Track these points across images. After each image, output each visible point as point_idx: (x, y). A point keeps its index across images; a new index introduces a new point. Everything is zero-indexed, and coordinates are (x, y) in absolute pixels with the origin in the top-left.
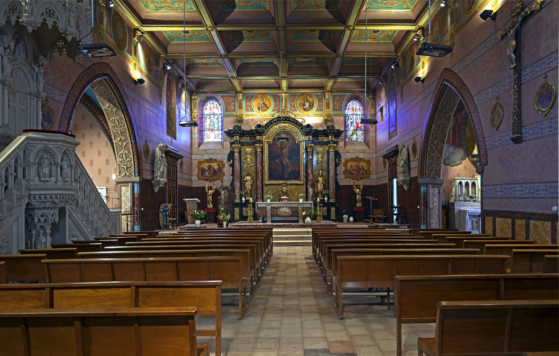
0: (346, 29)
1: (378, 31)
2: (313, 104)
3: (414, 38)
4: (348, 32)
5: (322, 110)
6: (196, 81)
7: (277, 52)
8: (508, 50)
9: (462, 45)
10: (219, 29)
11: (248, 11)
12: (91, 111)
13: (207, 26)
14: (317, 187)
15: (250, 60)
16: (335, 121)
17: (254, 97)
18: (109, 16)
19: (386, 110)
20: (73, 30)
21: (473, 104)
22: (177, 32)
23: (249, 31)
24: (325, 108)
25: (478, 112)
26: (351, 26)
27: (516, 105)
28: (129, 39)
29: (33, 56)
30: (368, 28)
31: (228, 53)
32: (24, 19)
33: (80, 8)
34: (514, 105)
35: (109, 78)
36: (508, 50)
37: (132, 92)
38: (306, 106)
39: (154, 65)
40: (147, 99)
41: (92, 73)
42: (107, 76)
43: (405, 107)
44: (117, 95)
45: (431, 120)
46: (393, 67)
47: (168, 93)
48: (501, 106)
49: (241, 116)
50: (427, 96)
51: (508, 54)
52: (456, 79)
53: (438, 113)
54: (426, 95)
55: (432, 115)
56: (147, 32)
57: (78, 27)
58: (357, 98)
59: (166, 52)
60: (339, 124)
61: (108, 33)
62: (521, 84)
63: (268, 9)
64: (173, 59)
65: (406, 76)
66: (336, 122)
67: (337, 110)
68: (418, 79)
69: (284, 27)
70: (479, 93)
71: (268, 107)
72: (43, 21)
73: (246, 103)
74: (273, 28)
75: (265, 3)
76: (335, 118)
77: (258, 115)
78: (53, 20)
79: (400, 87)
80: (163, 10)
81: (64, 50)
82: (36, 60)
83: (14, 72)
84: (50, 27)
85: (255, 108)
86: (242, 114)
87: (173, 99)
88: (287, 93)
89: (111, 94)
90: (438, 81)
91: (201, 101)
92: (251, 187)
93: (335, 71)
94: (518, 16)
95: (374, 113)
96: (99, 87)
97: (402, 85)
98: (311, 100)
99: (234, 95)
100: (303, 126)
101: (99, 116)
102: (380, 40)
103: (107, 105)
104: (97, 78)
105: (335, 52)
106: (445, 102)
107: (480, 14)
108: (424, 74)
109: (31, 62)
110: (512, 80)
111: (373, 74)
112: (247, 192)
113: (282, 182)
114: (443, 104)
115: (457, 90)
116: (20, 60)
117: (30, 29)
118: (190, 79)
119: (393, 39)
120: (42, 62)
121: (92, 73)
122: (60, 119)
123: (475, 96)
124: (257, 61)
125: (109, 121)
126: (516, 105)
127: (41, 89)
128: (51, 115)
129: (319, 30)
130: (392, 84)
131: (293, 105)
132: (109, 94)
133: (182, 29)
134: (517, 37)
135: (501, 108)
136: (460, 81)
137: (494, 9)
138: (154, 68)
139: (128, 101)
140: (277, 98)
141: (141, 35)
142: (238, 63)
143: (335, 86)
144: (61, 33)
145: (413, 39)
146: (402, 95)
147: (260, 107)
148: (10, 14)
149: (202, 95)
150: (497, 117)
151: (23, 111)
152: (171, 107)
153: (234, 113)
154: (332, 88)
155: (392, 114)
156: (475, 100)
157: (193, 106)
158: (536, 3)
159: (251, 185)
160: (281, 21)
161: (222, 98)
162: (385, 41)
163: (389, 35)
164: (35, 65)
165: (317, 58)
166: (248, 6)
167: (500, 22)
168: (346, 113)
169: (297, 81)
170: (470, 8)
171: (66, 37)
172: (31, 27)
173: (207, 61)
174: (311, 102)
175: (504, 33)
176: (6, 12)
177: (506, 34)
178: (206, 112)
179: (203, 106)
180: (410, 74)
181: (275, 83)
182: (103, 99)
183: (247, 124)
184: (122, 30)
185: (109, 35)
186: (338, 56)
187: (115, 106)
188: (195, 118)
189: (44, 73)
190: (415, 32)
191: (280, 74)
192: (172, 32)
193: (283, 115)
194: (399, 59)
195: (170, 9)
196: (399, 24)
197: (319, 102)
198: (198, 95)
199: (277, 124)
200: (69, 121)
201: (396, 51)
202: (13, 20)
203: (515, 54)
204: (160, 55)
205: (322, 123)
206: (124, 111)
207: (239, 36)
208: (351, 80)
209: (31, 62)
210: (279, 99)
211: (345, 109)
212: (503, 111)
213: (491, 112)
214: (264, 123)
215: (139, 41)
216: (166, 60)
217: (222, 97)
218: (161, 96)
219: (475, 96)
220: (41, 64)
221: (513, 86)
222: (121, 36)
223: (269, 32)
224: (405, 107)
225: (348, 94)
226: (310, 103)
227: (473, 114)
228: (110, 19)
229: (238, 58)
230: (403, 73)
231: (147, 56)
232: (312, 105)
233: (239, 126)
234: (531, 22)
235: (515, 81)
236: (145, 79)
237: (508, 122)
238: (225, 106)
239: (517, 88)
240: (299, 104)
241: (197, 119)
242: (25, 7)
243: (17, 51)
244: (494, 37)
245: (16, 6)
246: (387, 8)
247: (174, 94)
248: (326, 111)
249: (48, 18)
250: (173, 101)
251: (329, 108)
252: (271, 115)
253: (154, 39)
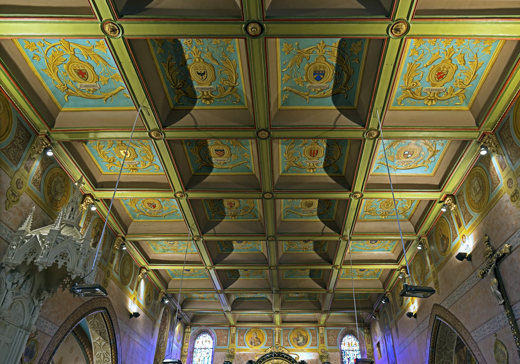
0: (333, 268)
1: (364, 270)
2: (307, 339)
3: (399, 275)
4: (336, 271)
5: (316, 345)
6: (191, 315)
7: (270, 289)
8: (491, 286)
9: (446, 282)
10: (217, 268)
11: (244, 253)
12: (81, 343)
13: (206, 266)
15: (245, 295)
16: (331, 357)
17: (247, 331)
18: (120, 257)
19: (383, 345)
20: (79, 270)
21: (472, 341)
22: (179, 270)
23: (244, 270)
24: (320, 343)
25: (479, 350)
26: (338, 266)
27: (518, 342)
28: (134, 276)
29: (38, 290)
30: (353, 267)
31: (224, 289)
32: (38, 260)
33: (92, 251)
34: (516, 343)
35: (106, 311)
36: (491, 286)
37: (125, 326)
38: (300, 341)
39: (153, 299)
40: (139, 332)
41: (90, 306)
42: (103, 310)
43: (402, 343)
44: (109, 328)
45: (432, 358)
46: (383, 302)
47: (162, 326)
48: (502, 343)
49: (233, 351)
50: (423, 332)
51: (493, 291)
52: (448, 315)
53: (438, 350)
54: (421, 330)
55: (432, 352)
56: (152, 270)
57: (85, 267)
58: (352, 333)
59: (167, 287)
60: (335, 360)
61: (115, 271)
62: (516, 320)
63: (262, 251)
64: (172, 294)
65: (398, 311)
66: (332, 359)
67: (332, 346)
68: (410, 315)
69: (276, 266)
70: (475, 329)
71: (261, 341)
72: (55, 262)
73: (239, 337)
74: (266, 268)
75: (259, 247)
76: (331, 354)
77: (250, 350)
78: (64, 261)
79: (393, 321)
80: (169, 252)
81: (68, 285)
82: (39, 294)
83: (14, 304)
84: (59, 267)
85: (248, 343)
86: (234, 349)
87: (166, 333)
88: (281, 327)
89: (104, 327)
90: (431, 317)
91: (193, 334)
93: (327, 304)
94: (492, 257)
95: (371, 348)
96: (94, 320)
97: (395, 320)
98: (305, 335)
99: (227, 328)
100: (297, 362)
101: (87, 350)
102: (367, 278)
103: (97, 338)
104: (94, 311)
105: (326, 288)
106: (442, 338)
107: (456, 256)
108: (415, 310)
109: (33, 296)
110: (505, 315)
111: (363, 309)
114: (440, 340)
115: (452, 326)
116: (23, 294)
117: (41, 268)
118: (186, 312)
119: (379, 276)
120: (44, 296)
121: (90, 306)
122: (42, 354)
123: (472, 332)
124: (251, 296)
125: (95, 355)
126: (518, 342)
127: (33, 322)
128: (35, 349)
129: (309, 269)
130: (385, 319)
131: (286, 339)
132: (102, 327)
133: (182, 268)
134: (497, 274)
135: (503, 346)
136: (453, 317)
137: (468, 252)
138: (153, 302)
139: (118, 335)
140: (270, 333)
141: (146, 272)
142: (233, 298)
143: (329, 320)
144: (68, 272)
145: (398, 277)
146: (397, 330)
147: (253, 341)
148: (28, 256)
149: (196, 328)
150: (501, 356)
151: (8, 344)
152: (162, 340)
153: (226, 347)
154: (325, 323)
155: (390, 350)
156: (473, 337)
157: (185, 339)
158: (505, 248)
160: (273, 261)
161: (215, 331)
162: (372, 278)
163: (375, 273)
164: (36, 298)
165: (309, 294)
166: (244, 249)
167: (477, 262)
168: (342, 349)
169: (290, 316)
170: (445, 251)
171: (71, 276)
172: (42, 267)
173: (204, 296)
174: (305, 337)
175: (483, 271)
176: (26, 255)
177: (485, 273)
178: (197, 346)
179: (196, 339)
180: (402, 309)
181: (268, 317)
182: (94, 332)
183: (238, 360)
184: (129, 268)
185: (116, 272)
186: (328, 292)
187: (105, 339)
188: (185, 352)
189: (43, 306)
190: (398, 270)
191: (273, 309)
192: (175, 270)
193: (276, 350)
194: (388, 294)
195: (175, 251)
196: (382, 264)
197: (313, 337)
198: (192, 328)
199: (269, 360)
200: (52, 355)
201: (384, 287)
202: (29, 261)
203: (500, 291)
204: (161, 290)
205: (317, 360)
206: (112, 345)
207: (235, 274)
208: (344, 314)
209: (33, 296)
210: (273, 333)
211: (341, 344)
212: (506, 349)
213: (493, 351)
214: (256, 359)
215: (143, 278)
216: (166, 295)
217: (215, 330)
218: (153, 329)
219: (472, 332)
220: (42, 298)
221: (508, 322)
222: (127, 273)
223: (263, 270)
224: (402, 343)
225: (343, 329)
226: (303, 338)
227: (475, 351)
228: (120, 259)
229: (233, 293)
230: (394, 308)
231: (148, 291)
232: (306, 339)
233: (229, 362)
234: (505, 262)
235: (508, 317)
236: (142, 313)
237: (515, 362)
238: (218, 340)
239: (512, 323)
240: (293, 339)
241: (187, 353)
242: (43, 251)
243: (24, 286)
244: (475, 276)
245: (36, 250)
246: (369, 250)
247: (168, 327)
248: (320, 347)
249: (61, 259)
250: (165, 334)
251: (323, 343)
252: (264, 350)
253: (157, 276)
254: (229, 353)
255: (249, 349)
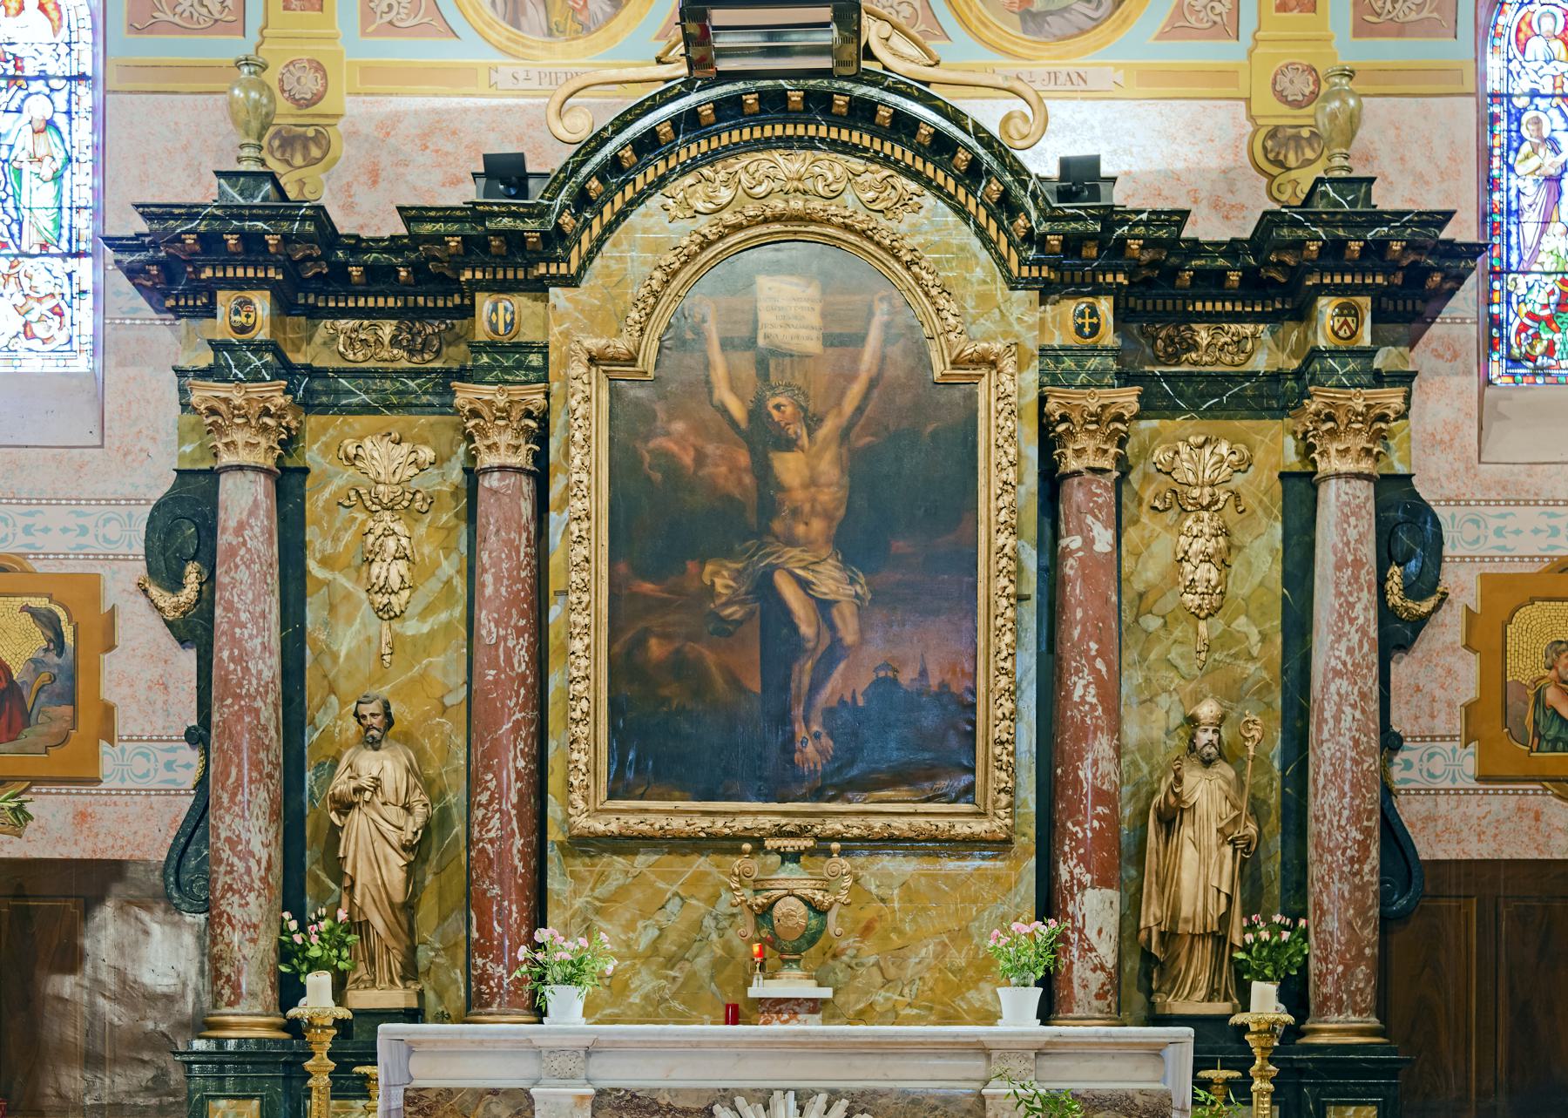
5: (1229, 28)
14: (1167, 880)
86: (319, 67)
92: (410, 869)
112: (359, 926)
113: (767, 822)
159: (406, 848)
199: (711, 158)
254: (263, 87)
255: (492, 69)
